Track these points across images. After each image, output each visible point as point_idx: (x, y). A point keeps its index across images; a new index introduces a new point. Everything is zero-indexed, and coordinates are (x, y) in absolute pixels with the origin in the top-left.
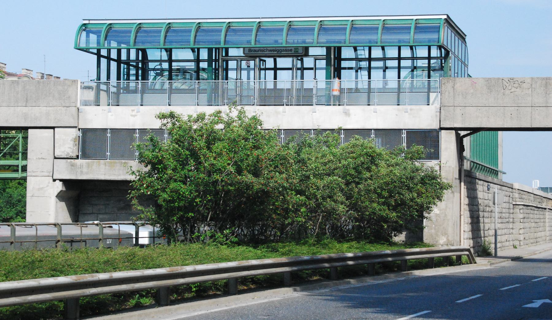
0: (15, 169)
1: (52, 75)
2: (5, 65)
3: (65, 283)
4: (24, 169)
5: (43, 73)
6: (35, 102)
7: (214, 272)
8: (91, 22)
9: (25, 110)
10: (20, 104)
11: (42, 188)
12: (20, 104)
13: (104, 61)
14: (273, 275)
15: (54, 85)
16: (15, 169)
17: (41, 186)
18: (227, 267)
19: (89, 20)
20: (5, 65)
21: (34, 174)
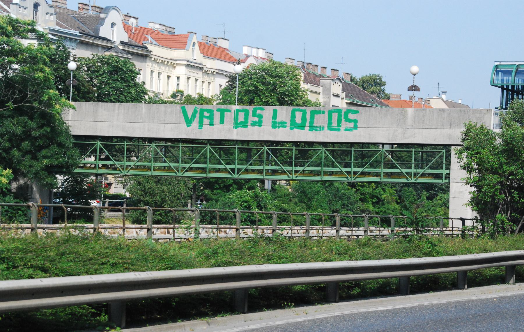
0: (438, 176)
1: (311, 64)
2: (272, 54)
3: (74, 284)
4: (448, 176)
5: (304, 61)
6: (458, 125)
7: (291, 275)
8: (502, 63)
9: (449, 132)
10: (445, 127)
11: (462, 192)
12: (445, 127)
13: (505, 91)
14: (220, 293)
15: (473, 113)
16: (438, 176)
17: (461, 190)
18: (189, 276)
19: (500, 62)
20: (174, 29)
21: (455, 181)
